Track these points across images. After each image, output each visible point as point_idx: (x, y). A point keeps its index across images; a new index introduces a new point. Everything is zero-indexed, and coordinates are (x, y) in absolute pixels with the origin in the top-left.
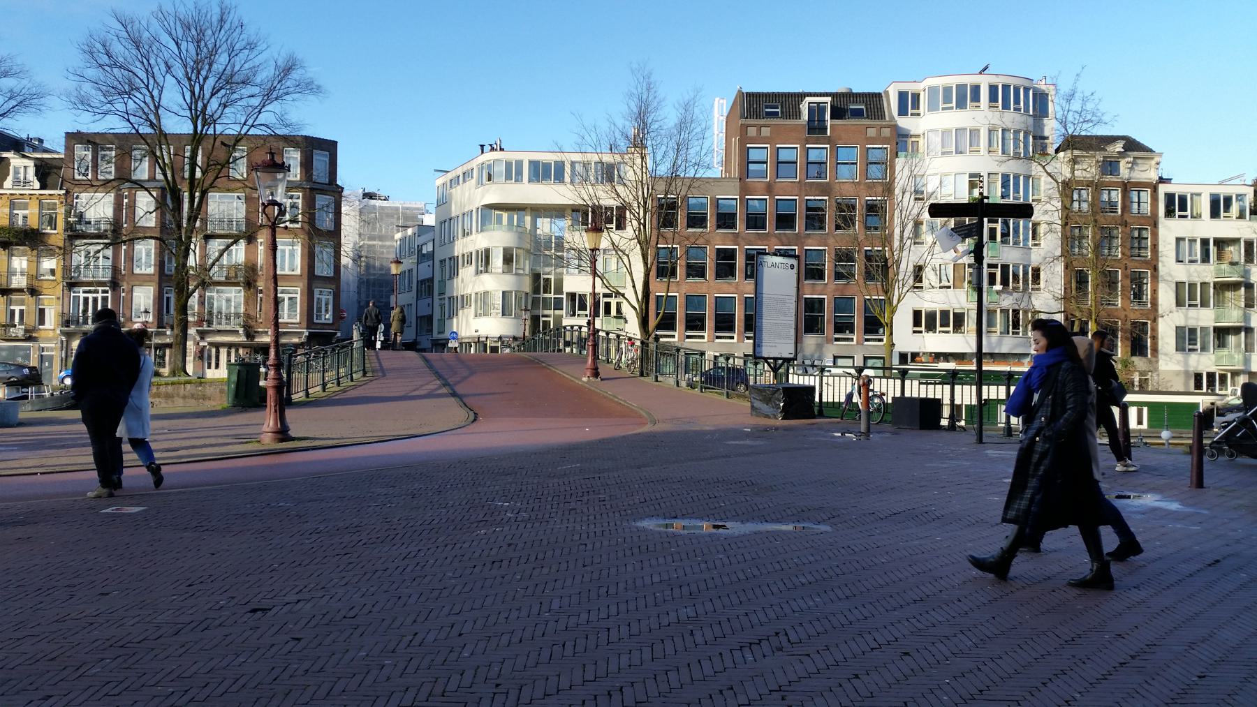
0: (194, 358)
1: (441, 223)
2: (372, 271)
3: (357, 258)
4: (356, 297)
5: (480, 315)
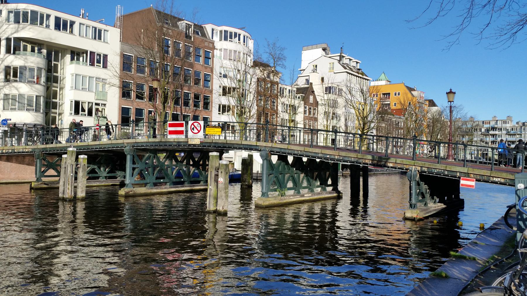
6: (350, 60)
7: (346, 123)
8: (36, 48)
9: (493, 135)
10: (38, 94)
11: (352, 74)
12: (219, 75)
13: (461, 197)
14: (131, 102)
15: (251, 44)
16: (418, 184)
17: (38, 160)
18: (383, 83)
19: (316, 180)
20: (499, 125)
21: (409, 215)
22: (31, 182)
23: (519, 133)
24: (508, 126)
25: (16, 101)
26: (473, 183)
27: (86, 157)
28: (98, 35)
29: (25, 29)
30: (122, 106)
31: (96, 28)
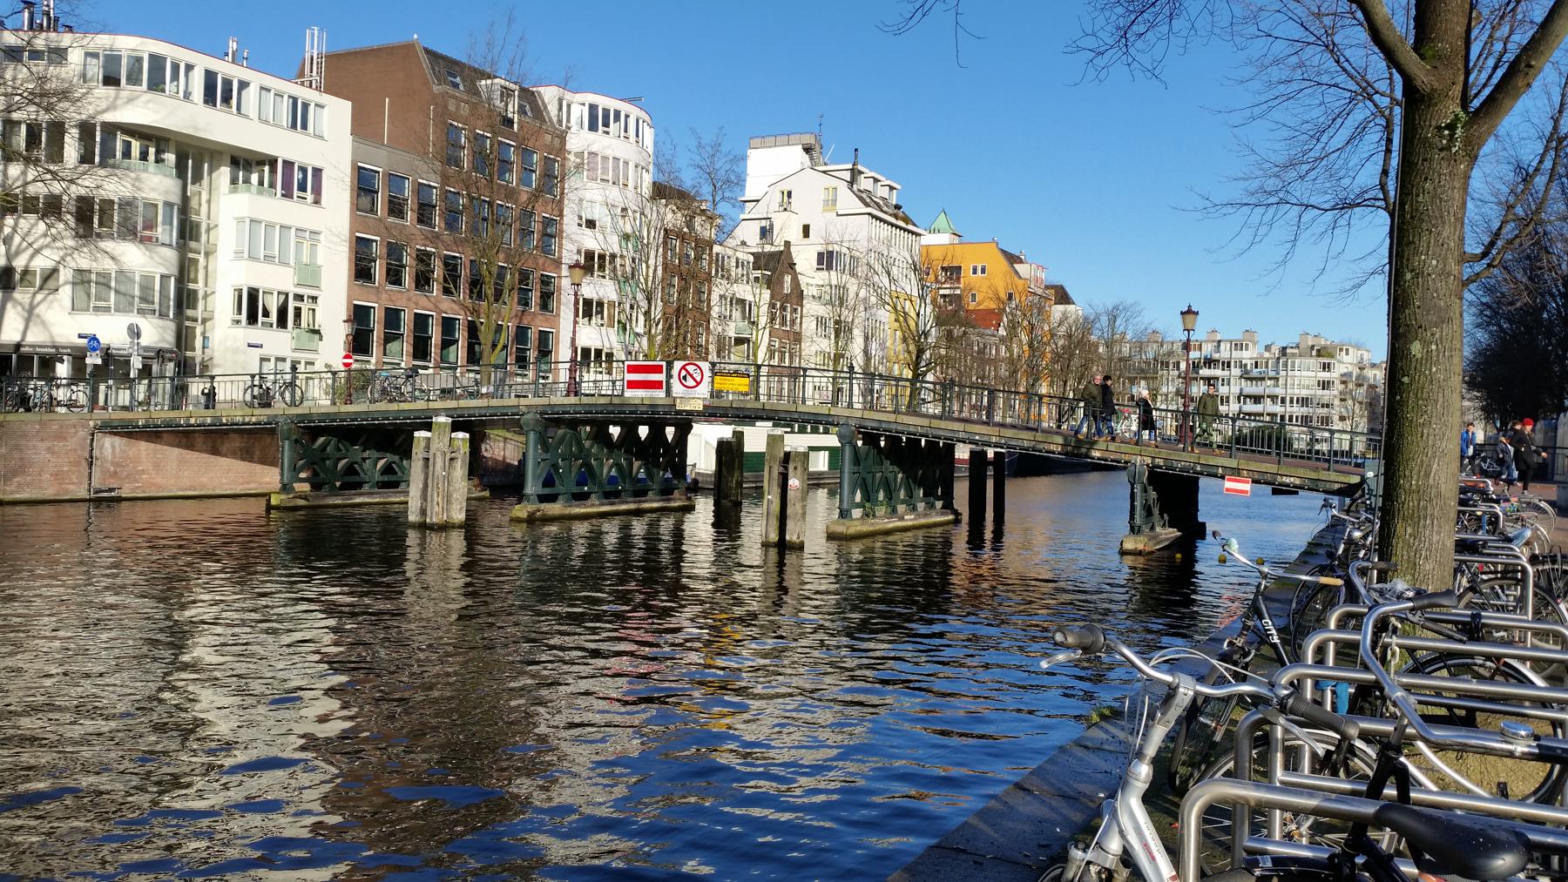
6: (876, 180)
7: (866, 346)
8: (152, 150)
9: (1209, 381)
11: (881, 220)
12: (578, 221)
13: (1200, 520)
14: (374, 291)
15: (648, 135)
16: (1145, 491)
17: (287, 442)
18: (944, 239)
19: (919, 487)
20: (1224, 354)
21: (1129, 546)
22: (267, 495)
23: (1272, 374)
24: (1247, 356)
25: (110, 287)
26: (1247, 487)
27: (468, 435)
28: (299, 118)
29: (135, 103)
30: (356, 302)
31: (295, 100)
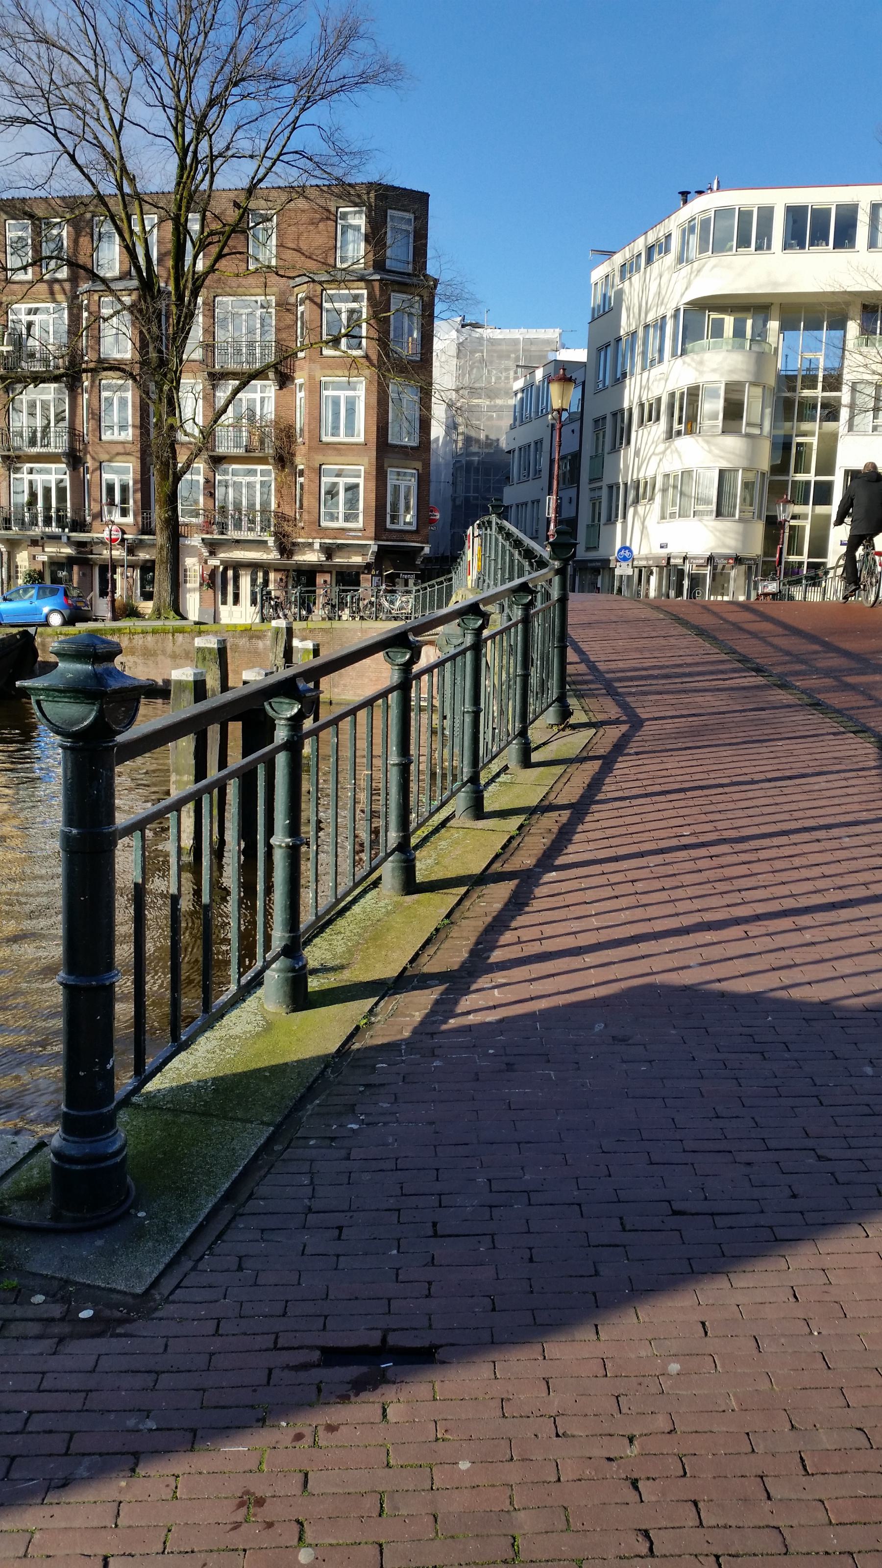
0: (201, 585)
1: (599, 350)
2: (474, 449)
3: (452, 427)
4: (450, 491)
5: (672, 516)
10: (725, 464)
